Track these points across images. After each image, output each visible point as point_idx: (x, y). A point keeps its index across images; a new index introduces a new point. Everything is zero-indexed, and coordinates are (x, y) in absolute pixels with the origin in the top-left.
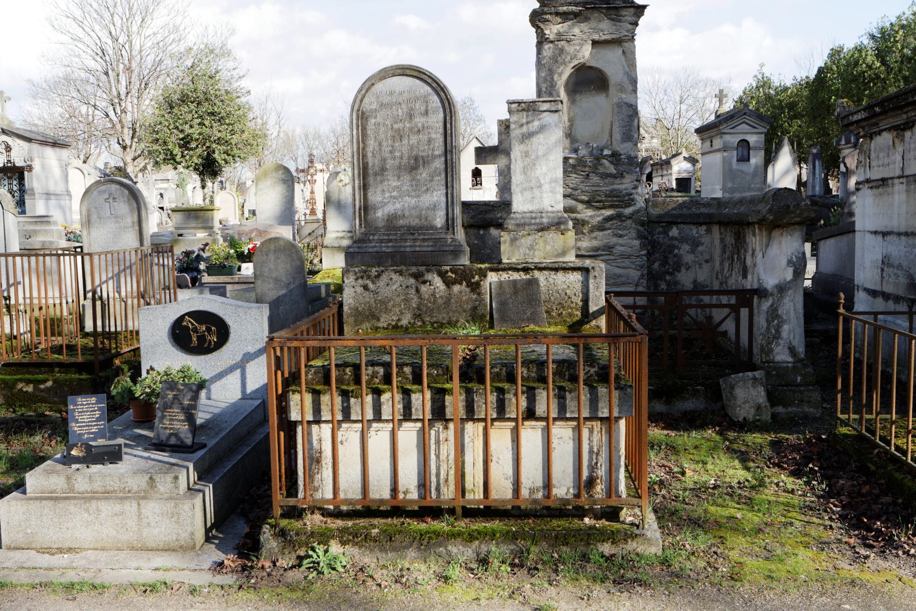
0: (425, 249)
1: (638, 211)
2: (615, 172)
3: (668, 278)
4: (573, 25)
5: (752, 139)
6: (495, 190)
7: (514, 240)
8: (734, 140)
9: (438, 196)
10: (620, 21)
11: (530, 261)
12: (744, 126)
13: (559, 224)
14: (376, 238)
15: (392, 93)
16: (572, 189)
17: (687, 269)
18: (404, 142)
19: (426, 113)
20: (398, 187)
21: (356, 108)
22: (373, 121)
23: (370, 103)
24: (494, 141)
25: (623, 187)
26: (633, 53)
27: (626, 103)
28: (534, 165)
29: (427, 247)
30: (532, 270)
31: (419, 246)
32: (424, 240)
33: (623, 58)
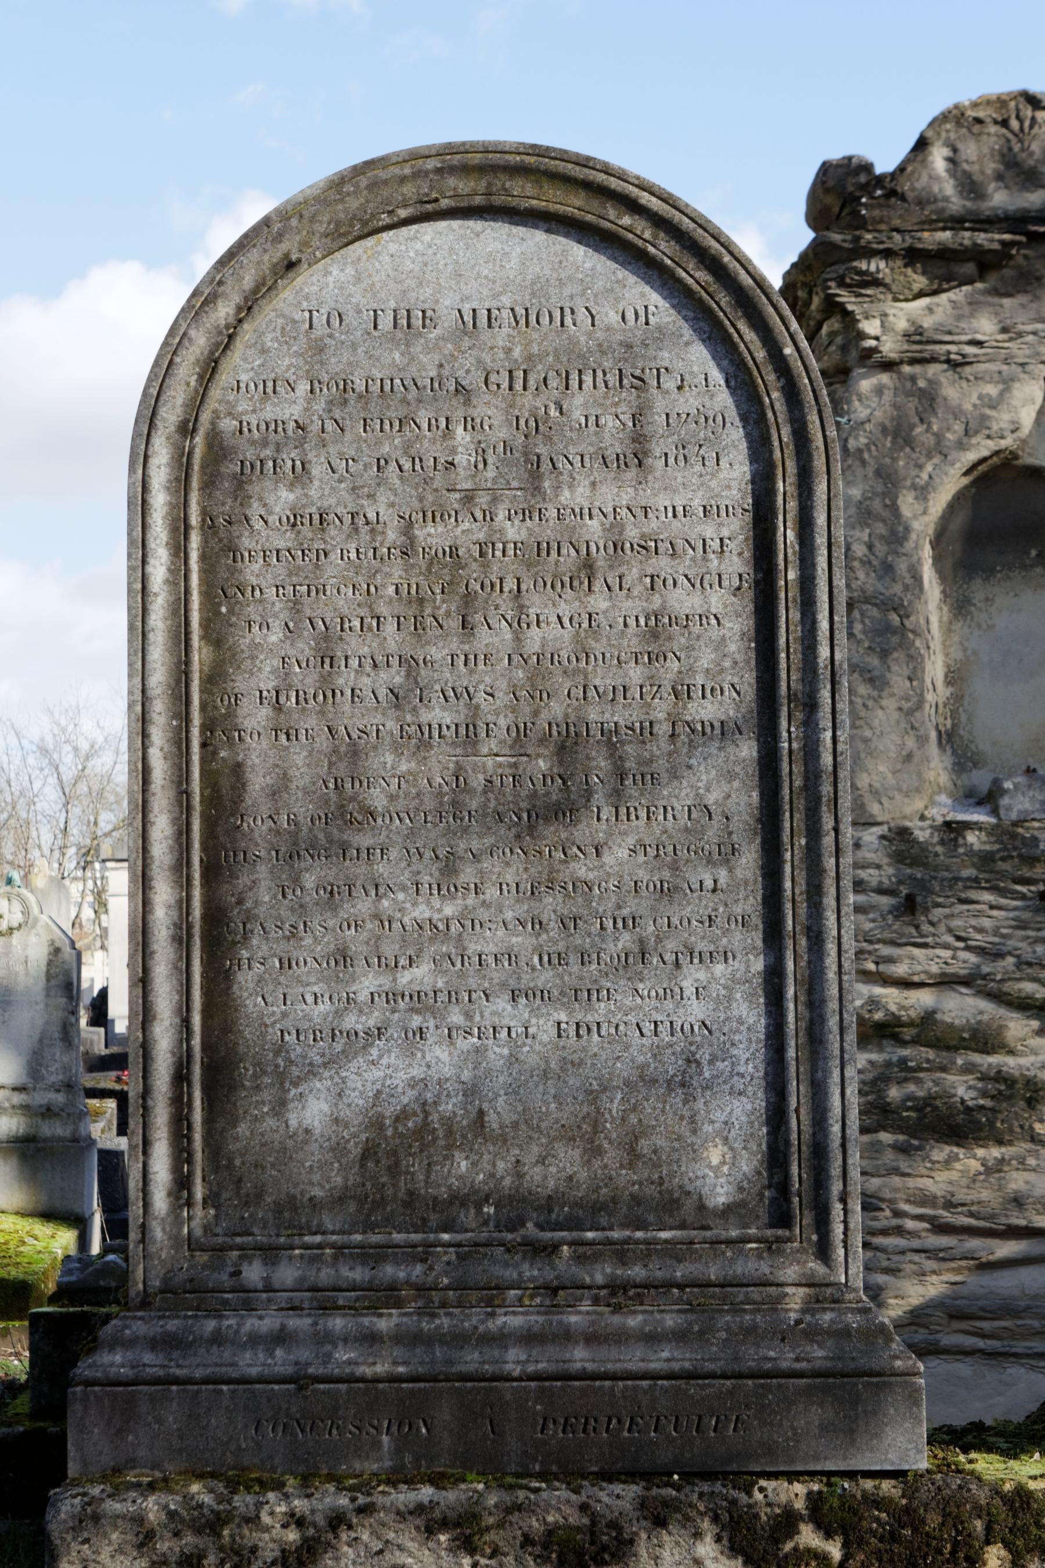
0: (633, 1358)
4: (973, 304)
9: (716, 994)
14: (287, 1274)
15: (410, 323)
16: (980, 951)
18: (484, 638)
19: (637, 455)
20: (438, 930)
21: (171, 415)
22: (283, 498)
23: (264, 386)
29: (647, 1345)
31: (592, 1338)
32: (619, 1295)
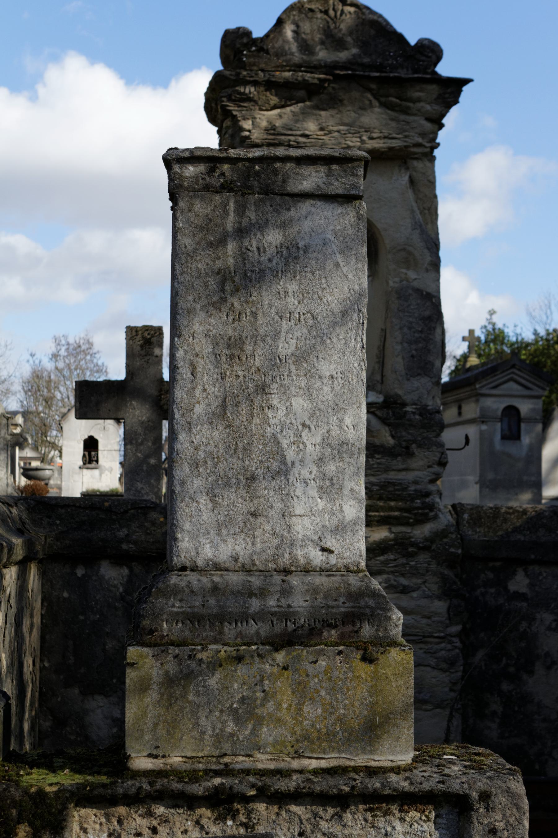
1: (442, 534)
2: (391, 441)
3: (505, 686)
5: (525, 407)
6: (117, 471)
7: (175, 684)
8: (496, 405)
10: (406, 111)
11: (241, 762)
12: (512, 385)
13: (352, 618)
17: (549, 668)
24: (117, 371)
25: (410, 476)
26: (432, 183)
27: (418, 291)
28: (262, 389)
30: (246, 800)
33: (410, 194)
